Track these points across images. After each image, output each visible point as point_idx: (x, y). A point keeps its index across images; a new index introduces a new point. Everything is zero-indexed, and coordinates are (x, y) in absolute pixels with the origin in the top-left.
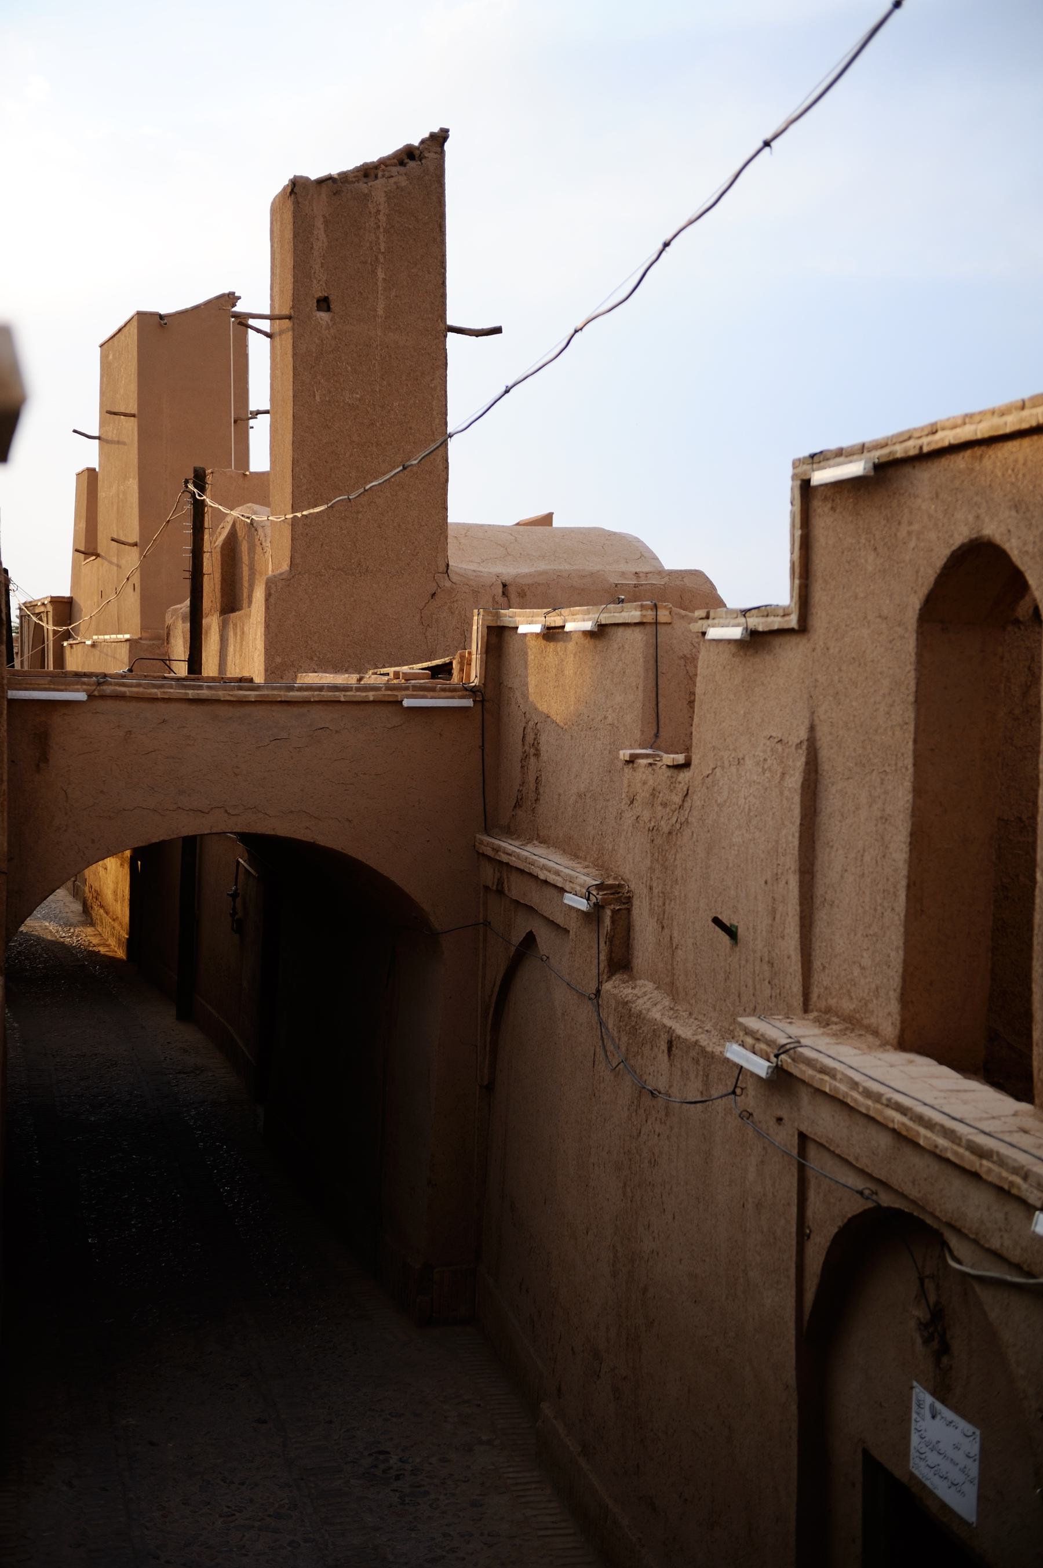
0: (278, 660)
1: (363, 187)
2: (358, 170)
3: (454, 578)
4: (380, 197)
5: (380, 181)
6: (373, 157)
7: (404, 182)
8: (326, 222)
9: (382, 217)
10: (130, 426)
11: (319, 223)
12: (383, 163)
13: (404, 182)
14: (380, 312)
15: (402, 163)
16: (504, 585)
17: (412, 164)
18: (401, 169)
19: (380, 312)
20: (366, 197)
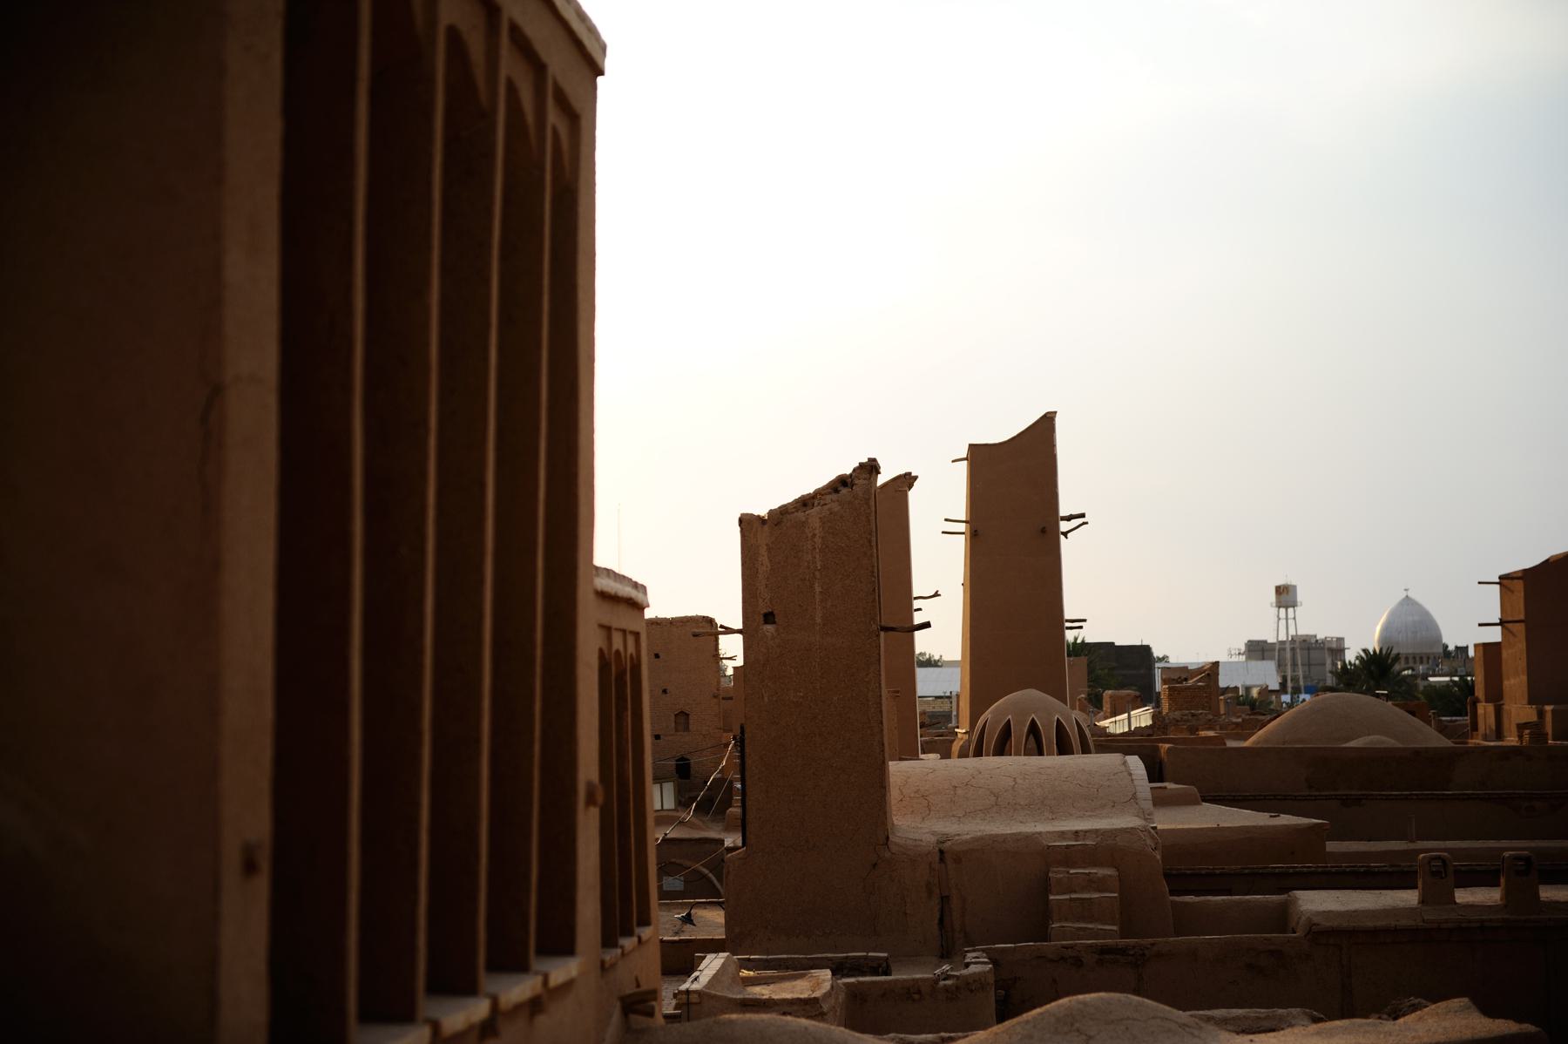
0: (737, 930)
1: (800, 515)
2: (796, 501)
3: (894, 849)
4: (815, 523)
5: (817, 509)
6: (809, 488)
7: (836, 507)
8: (769, 550)
9: (818, 540)
10: (1520, 629)
11: (763, 551)
12: (819, 494)
13: (836, 507)
14: (819, 620)
15: (836, 491)
16: (941, 852)
17: (844, 491)
18: (834, 496)
19: (819, 620)
20: (804, 524)
